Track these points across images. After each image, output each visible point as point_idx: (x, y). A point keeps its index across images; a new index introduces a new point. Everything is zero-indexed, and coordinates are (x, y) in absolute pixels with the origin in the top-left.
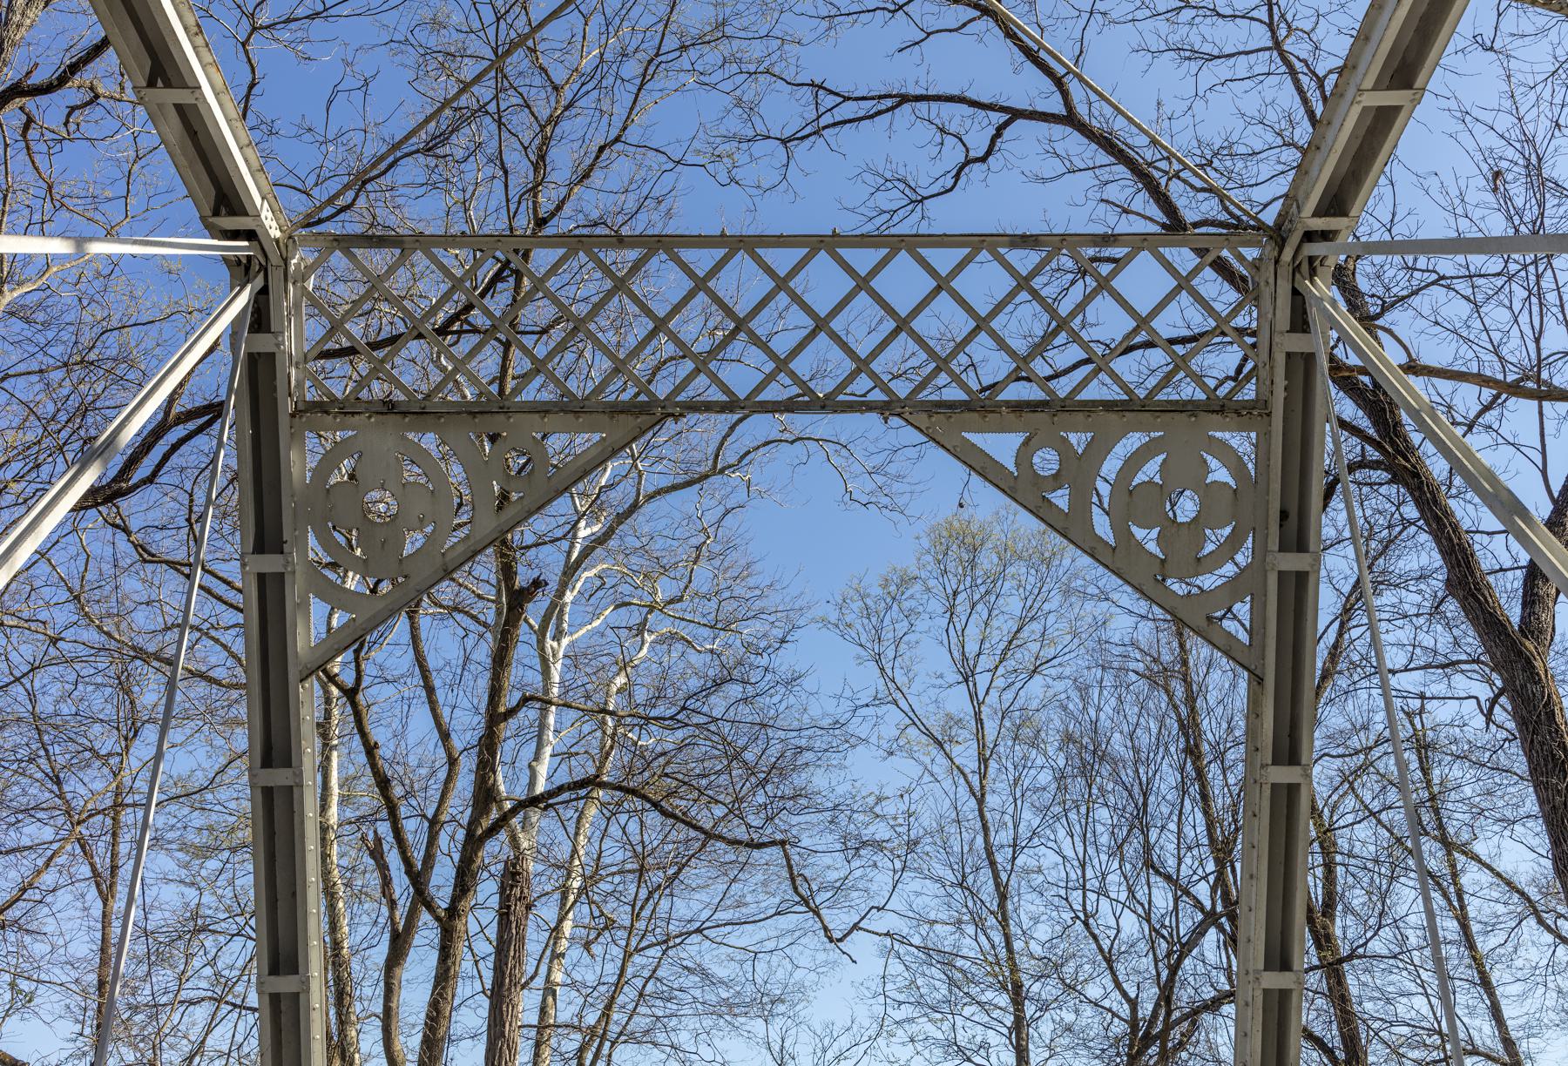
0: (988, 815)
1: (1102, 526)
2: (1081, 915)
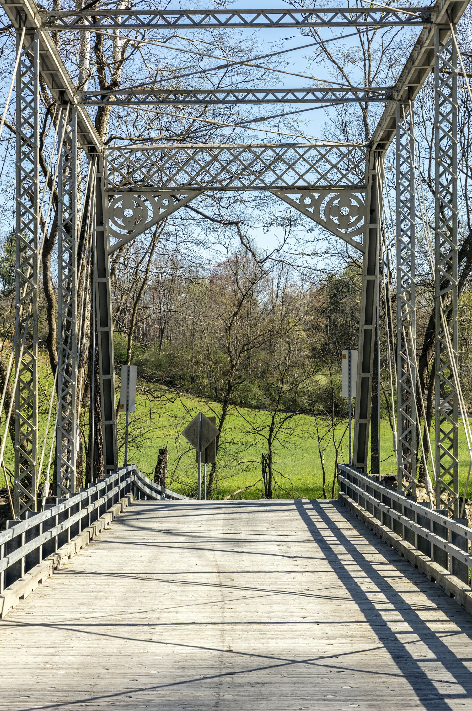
0: (368, 119)
1: (323, 217)
2: (427, 179)
